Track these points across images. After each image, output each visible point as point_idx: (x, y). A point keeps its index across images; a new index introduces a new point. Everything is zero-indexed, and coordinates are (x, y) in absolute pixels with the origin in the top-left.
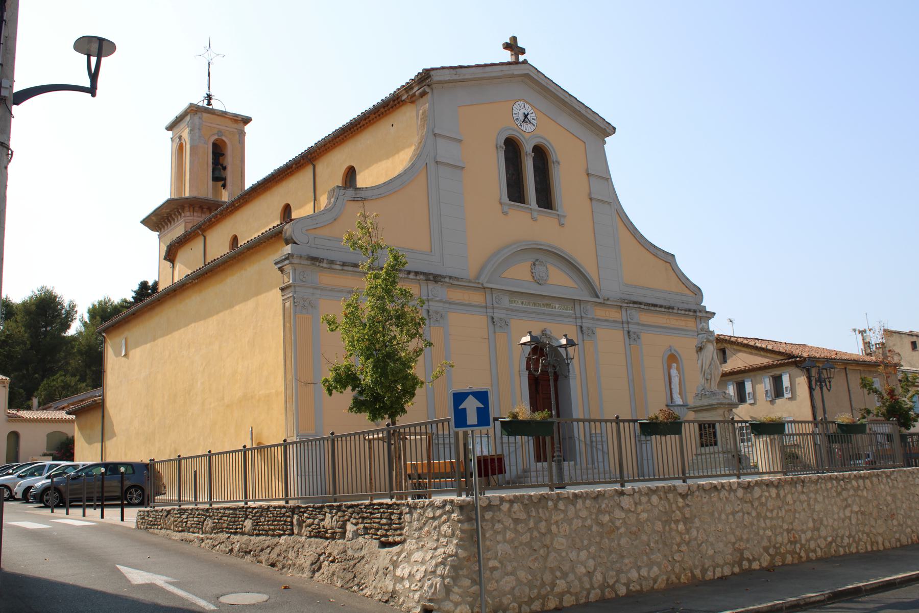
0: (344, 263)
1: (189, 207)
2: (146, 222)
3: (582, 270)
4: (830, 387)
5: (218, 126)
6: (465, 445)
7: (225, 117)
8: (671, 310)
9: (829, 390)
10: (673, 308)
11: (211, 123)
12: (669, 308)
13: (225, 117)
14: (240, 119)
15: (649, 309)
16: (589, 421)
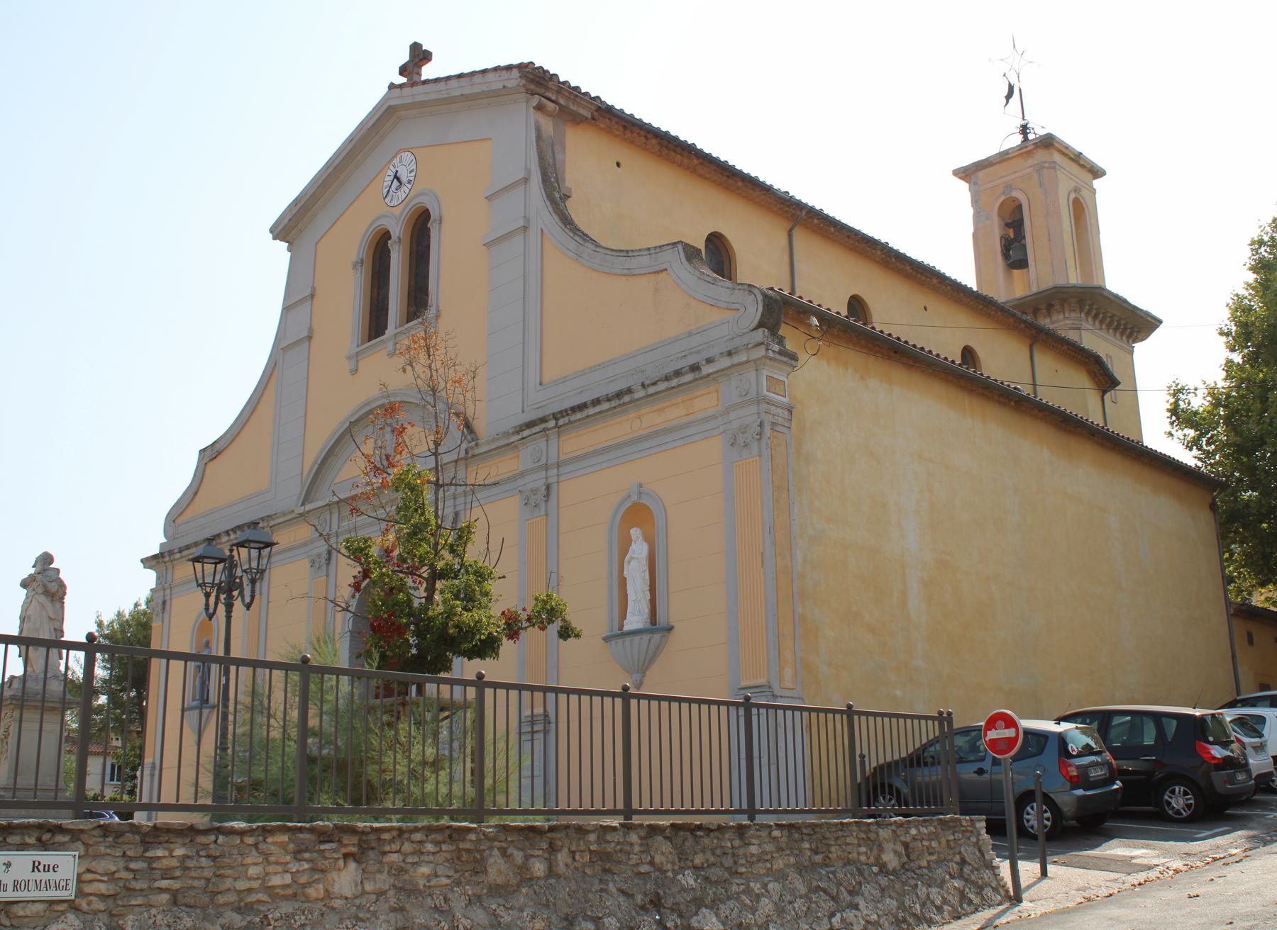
0: (180, 548)
1: (1062, 306)
2: (142, 561)
3: (323, 456)
4: (253, 597)
5: (1003, 180)
6: (862, 757)
7: (1009, 159)
8: (626, 399)
9: (248, 606)
10: (629, 391)
11: (991, 182)
12: (619, 395)
13: (1009, 159)
14: (1033, 147)
15: (570, 422)
16: (557, 691)
